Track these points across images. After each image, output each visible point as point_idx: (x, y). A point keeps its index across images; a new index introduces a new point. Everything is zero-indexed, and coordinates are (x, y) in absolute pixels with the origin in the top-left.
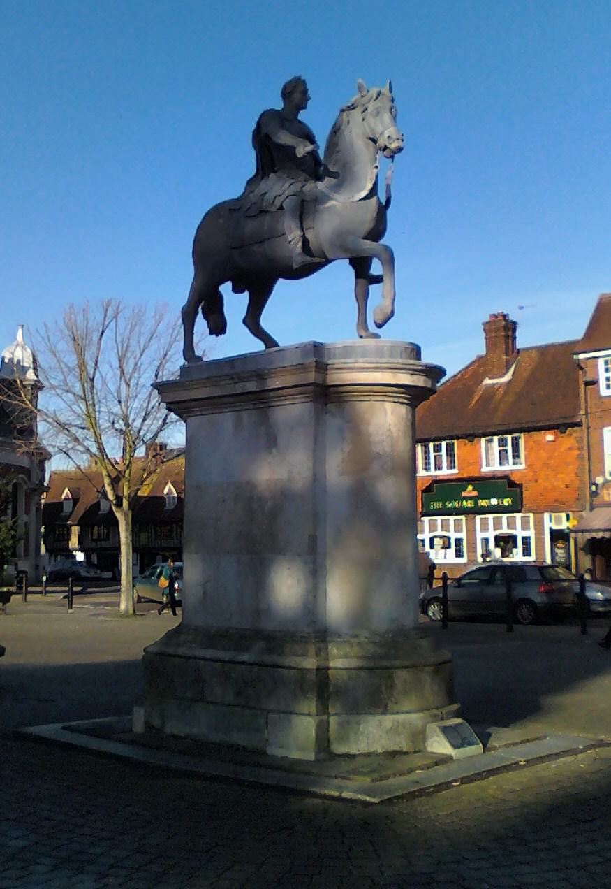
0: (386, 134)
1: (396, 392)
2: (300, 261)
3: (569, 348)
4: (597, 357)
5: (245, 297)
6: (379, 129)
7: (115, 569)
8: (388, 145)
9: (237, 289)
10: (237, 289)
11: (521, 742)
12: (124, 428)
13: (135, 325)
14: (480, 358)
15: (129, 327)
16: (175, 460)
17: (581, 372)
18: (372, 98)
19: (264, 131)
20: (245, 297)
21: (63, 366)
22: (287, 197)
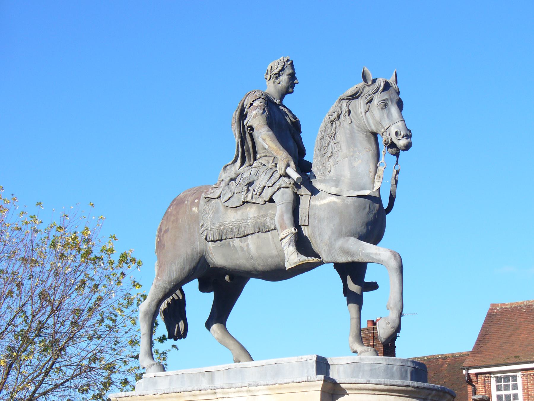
0: (393, 130)
1: (364, 389)
2: (296, 261)
3: (456, 362)
4: (490, 373)
5: (210, 297)
6: (386, 123)
7: (260, 276)
8: (395, 141)
9: (203, 288)
10: (203, 288)
11: (277, 190)
12: (92, 256)
13: (166, 231)
14: (304, 154)
15: (52, 359)
16: (293, 230)
17: (470, 388)
18: (378, 88)
19: (404, 148)
20: (210, 297)
21: (64, 264)
22: (279, 189)
